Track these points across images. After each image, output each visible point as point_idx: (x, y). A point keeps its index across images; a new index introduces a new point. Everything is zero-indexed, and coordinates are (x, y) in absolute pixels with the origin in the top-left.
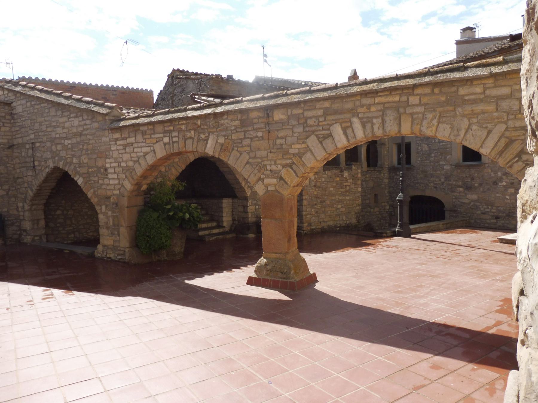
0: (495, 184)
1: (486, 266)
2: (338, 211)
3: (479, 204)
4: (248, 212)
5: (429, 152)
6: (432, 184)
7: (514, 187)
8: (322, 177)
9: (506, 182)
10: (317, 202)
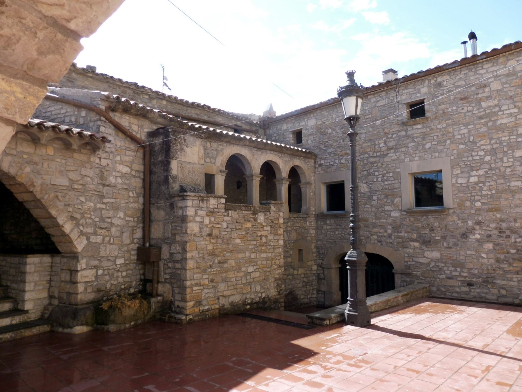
0: (465, 236)
2: (248, 277)
3: (443, 265)
4: (76, 283)
5: (369, 194)
6: (375, 237)
7: (493, 242)
8: (223, 221)
9: (479, 234)
10: (213, 264)
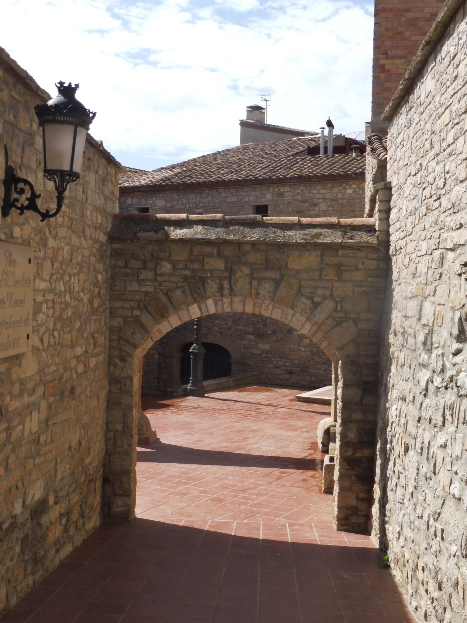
0: (290, 332)
1: (292, 423)
6: (217, 328)
